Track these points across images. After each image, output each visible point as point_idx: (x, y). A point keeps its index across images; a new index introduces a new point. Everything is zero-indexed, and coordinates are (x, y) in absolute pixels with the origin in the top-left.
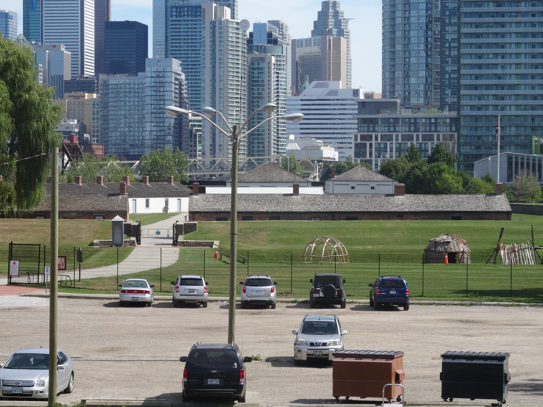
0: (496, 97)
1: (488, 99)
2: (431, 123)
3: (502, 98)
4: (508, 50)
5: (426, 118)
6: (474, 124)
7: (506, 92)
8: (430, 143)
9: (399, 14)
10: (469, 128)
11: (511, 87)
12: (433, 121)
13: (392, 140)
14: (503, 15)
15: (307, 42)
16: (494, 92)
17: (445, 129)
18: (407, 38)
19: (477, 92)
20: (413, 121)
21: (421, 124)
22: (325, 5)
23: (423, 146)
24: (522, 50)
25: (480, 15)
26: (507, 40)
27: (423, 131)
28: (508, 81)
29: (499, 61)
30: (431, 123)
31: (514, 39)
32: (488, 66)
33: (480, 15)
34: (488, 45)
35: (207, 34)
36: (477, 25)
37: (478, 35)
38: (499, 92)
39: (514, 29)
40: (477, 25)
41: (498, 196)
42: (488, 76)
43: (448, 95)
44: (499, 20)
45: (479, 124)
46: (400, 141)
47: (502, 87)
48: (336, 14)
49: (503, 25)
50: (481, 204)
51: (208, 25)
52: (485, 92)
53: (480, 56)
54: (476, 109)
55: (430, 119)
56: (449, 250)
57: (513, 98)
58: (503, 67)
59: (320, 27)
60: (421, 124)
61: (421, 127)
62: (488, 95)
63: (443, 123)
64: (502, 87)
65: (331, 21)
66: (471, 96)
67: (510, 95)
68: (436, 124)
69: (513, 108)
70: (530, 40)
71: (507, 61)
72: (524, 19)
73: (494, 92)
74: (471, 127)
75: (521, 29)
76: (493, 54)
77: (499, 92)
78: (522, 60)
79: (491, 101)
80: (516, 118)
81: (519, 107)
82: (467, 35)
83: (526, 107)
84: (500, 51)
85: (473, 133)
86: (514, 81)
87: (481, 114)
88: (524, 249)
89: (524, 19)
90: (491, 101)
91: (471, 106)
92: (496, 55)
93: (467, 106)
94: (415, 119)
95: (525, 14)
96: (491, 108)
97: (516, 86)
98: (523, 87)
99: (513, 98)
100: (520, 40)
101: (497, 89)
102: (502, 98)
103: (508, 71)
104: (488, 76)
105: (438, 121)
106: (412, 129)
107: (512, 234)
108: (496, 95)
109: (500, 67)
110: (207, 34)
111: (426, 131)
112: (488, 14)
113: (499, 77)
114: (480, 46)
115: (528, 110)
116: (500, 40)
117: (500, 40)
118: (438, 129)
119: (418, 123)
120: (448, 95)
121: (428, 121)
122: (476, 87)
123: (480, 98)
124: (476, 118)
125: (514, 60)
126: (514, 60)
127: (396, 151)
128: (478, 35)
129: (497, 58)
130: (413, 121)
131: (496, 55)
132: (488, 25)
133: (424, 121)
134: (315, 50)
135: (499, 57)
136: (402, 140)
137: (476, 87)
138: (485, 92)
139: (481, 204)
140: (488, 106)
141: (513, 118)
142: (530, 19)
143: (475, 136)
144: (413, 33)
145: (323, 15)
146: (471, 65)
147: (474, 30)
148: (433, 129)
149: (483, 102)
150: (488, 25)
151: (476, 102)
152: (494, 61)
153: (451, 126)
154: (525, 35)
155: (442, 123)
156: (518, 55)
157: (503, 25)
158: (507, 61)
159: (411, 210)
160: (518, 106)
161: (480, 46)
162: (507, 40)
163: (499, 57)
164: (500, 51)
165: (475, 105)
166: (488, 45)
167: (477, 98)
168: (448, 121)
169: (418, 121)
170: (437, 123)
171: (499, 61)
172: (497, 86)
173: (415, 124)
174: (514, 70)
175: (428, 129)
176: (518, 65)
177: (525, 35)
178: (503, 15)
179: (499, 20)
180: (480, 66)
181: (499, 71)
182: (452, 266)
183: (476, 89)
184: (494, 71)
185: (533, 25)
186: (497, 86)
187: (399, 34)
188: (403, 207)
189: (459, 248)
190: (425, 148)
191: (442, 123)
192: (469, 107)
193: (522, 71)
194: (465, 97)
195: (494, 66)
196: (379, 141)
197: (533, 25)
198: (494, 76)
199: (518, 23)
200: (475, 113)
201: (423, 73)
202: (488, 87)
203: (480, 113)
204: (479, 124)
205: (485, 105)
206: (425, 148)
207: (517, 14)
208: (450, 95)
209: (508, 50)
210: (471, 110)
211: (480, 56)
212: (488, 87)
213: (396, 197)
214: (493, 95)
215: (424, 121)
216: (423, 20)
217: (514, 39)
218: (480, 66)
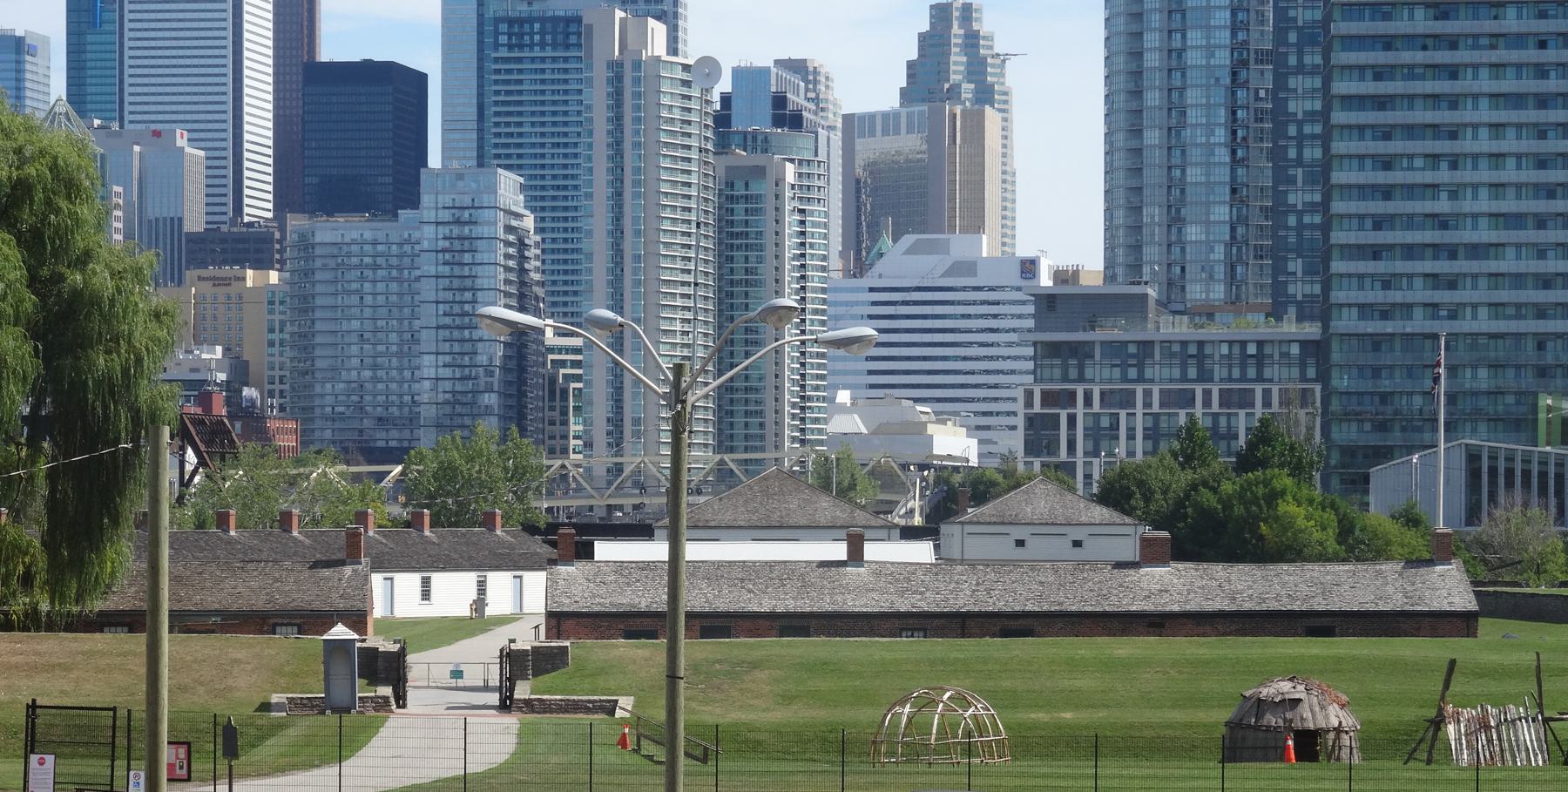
0: (1434, 280)
2: (1245, 356)
3: (1452, 283)
4: (1467, 145)
5: (1231, 343)
6: (1369, 359)
7: (1462, 266)
8: (1242, 413)
9: (1152, 40)
11: (1477, 251)
12: (1252, 349)
14: (1453, 43)
15: (889, 122)
16: (1428, 266)
18: (1176, 109)
19: (1381, 267)
20: (1192, 350)
21: (1217, 357)
22: (940, 15)
23: (1223, 421)
24: (1509, 144)
25: (1388, 43)
26: (1466, 115)
28: (1467, 236)
29: (1444, 175)
30: (1245, 356)
31: (1485, 114)
32: (1411, 191)
33: (1388, 43)
34: (1411, 131)
35: (598, 97)
36: (1379, 74)
38: (1443, 266)
39: (1486, 84)
40: (1379, 74)
41: (1439, 568)
42: (1410, 221)
44: (1443, 57)
45: (1386, 359)
47: (1452, 252)
48: (973, 40)
49: (1453, 72)
50: (1390, 589)
51: (600, 73)
52: (1401, 266)
53: (1387, 163)
55: (1243, 344)
56: (1297, 725)
57: (1483, 282)
58: (1454, 195)
59: (926, 78)
60: (1217, 357)
61: (1217, 367)
62: (1410, 276)
63: (1281, 355)
64: (1452, 252)
65: (957, 61)
66: (1361, 277)
67: (1475, 276)
68: (1260, 359)
69: (1483, 312)
72: (1514, 56)
73: (1428, 266)
74: (1361, 368)
75: (1508, 85)
76: (1426, 156)
77: (1443, 266)
78: (1509, 174)
79: (1420, 294)
81: (1500, 309)
82: (1350, 101)
83: (1520, 310)
85: (1367, 385)
86: (1485, 234)
88: (1513, 721)
89: (1514, 56)
90: (1420, 294)
91: (1361, 306)
92: (1434, 159)
93: (1350, 305)
94: (1201, 344)
95: (1519, 40)
96: (1418, 313)
97: (1492, 250)
99: (1483, 282)
100: (1503, 116)
102: (1452, 283)
103: (1467, 206)
104: (1410, 221)
105: (1267, 350)
106: (1192, 373)
108: (1435, 276)
109: (1444, 195)
110: (598, 97)
111: (1230, 380)
114: (1387, 134)
116: (1444, 116)
117: (1444, 116)
118: (1267, 373)
121: (1236, 350)
122: (1375, 252)
123: (1387, 283)
124: (1377, 342)
125: (1485, 175)
126: (1485, 175)
129: (1435, 168)
130: (1192, 350)
131: (1434, 159)
132: (1411, 72)
133: (1225, 349)
137: (1375, 252)
138: (1401, 266)
139: (1390, 589)
142: (1532, 55)
143: (1372, 394)
145: (933, 44)
146: (1360, 187)
147: (1370, 87)
149: (1396, 296)
150: (1411, 72)
151: (1376, 296)
152: (1428, 177)
153: (1303, 366)
154: (1516, 100)
155: (1276, 357)
156: (1497, 158)
157: (1453, 72)
158: (1466, 175)
159: (1188, 608)
160: (1496, 308)
161: (1387, 134)
162: (1466, 115)
163: (1444, 165)
165: (1371, 305)
166: (1411, 131)
167: (1378, 285)
168: (1295, 350)
169: (1208, 350)
170: (1205, 356)
171: (1444, 175)
172: (1437, 250)
173: (1201, 358)
174: (1484, 204)
175: (1236, 373)
176: (1497, 188)
177: (1516, 100)
178: (1453, 43)
179: (1443, 57)
180: (1387, 192)
181: (1443, 205)
182: (1308, 769)
184: (1429, 206)
185: (1541, 71)
186: (1437, 250)
187: (1153, 98)
188: (1166, 598)
189: (1327, 717)
190: (1229, 427)
191: (1276, 357)
193: (1509, 205)
194: (1345, 281)
195: (1429, 192)
199: (1497, 68)
201: (1222, 213)
202: (1410, 251)
203: (1389, 327)
204: (1386, 359)
206: (1229, 427)
207: (1496, 40)
208: (1300, 274)
209: (1467, 145)
210: (1362, 317)
211: (1387, 163)
212: (1410, 251)
215: (1225, 349)
216: (1223, 58)
217: (1485, 114)
218: (1387, 192)
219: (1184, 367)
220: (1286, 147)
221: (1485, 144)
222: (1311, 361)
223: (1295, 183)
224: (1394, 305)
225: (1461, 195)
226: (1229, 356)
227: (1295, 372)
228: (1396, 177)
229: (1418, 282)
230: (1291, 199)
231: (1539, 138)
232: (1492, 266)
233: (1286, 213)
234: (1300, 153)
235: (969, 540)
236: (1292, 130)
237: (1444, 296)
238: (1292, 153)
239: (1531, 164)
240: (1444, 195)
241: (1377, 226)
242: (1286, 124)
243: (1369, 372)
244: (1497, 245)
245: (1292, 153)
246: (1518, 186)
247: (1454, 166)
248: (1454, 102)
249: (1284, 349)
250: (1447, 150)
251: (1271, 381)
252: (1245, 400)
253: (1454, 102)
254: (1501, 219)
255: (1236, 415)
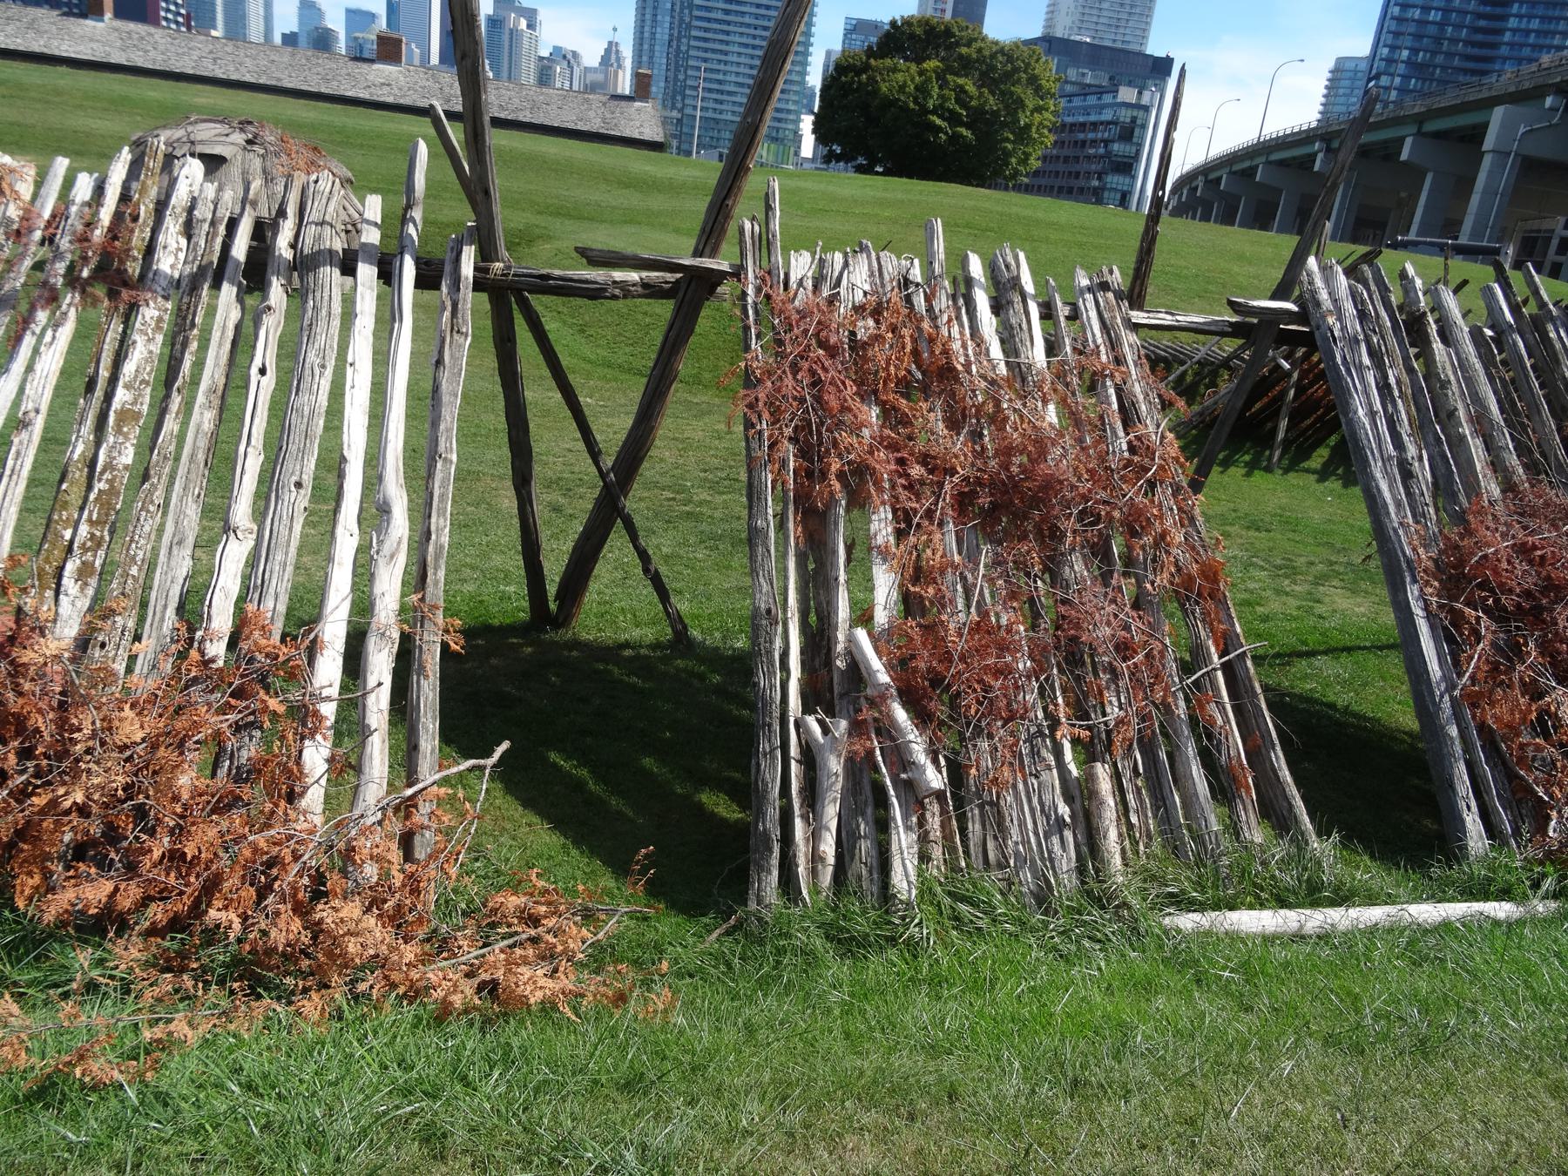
0: (716, 101)
3: (721, 102)
7: (725, 97)
9: (647, 29)
11: (730, 93)
14: (729, 23)
15: (595, 70)
18: (652, 51)
22: (610, 43)
24: (742, 60)
25: (709, 20)
29: (722, 67)
31: (736, 49)
33: (709, 20)
34: (714, 51)
35: (506, 37)
36: (706, 30)
37: (706, 40)
39: (737, 39)
40: (706, 30)
41: (637, 104)
44: (725, 27)
47: (722, 92)
49: (728, 33)
50: (592, 114)
51: (507, 32)
59: (605, 60)
64: (722, 92)
65: (613, 56)
70: (750, 51)
71: (728, 68)
75: (744, 40)
78: (742, 70)
82: (696, 38)
84: (723, 57)
86: (732, 88)
88: (304, 265)
92: (720, 61)
95: (748, 26)
100: (742, 50)
102: (721, 102)
107: (627, 186)
110: (506, 37)
112: (717, 21)
113: (720, 82)
114: (706, 50)
116: (723, 47)
117: (723, 47)
125: (734, 69)
126: (734, 69)
128: (706, 40)
132: (715, 31)
134: (600, 77)
139: (592, 114)
144: (657, 48)
145: (608, 51)
150: (715, 31)
154: (746, 46)
156: (738, 64)
157: (728, 33)
158: (728, 68)
159: (401, 101)
161: (706, 50)
164: (723, 57)
166: (714, 51)
171: (722, 67)
172: (718, 91)
174: (733, 78)
176: (737, 74)
177: (746, 46)
178: (729, 23)
179: (725, 27)
181: (721, 77)
185: (754, 37)
186: (718, 91)
187: (646, 47)
188: (386, 90)
197: (754, 37)
201: (662, 84)
207: (742, 24)
213: (376, 66)
217: (736, 49)
221: (735, 59)
237: (718, 106)
248: (727, 43)
253: (727, 43)
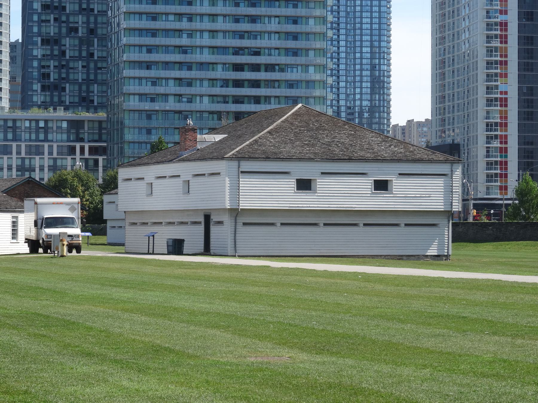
0: (179, 81)
1: (167, 85)
2: (38, 128)
3: (189, 83)
5: (30, 121)
6: (144, 123)
8: (37, 157)
10: (137, 131)
11: (202, 65)
12: (42, 124)
13: (43, 154)
16: (177, 74)
17: (59, 137)
19: (153, 73)
20: (10, 124)
21: (23, 128)
23: (27, 162)
27: (25, 141)
28: (197, 57)
29: (184, 24)
30: (38, 128)
32: (167, 32)
38: (184, 74)
42: (167, 48)
43: (37, 91)
45: (154, 123)
46: (55, 155)
47: (189, 67)
52: (163, 74)
53: (154, 17)
54: (149, 99)
55: (37, 121)
57: (206, 83)
58: (190, 36)
60: (23, 128)
61: (23, 133)
62: (167, 79)
63: (58, 127)
64: (189, 67)
66: (140, 78)
67: (201, 80)
68: (46, 130)
69: (206, 99)
71: (197, 25)
73: (177, 74)
74: (140, 129)
76: (175, 14)
77: (184, 74)
78: (220, 24)
79: (172, 88)
80: (211, 116)
81: (215, 98)
83: (225, 99)
85: (144, 138)
86: (206, 57)
87: (157, 108)
90: (172, 88)
91: (140, 95)
92: (179, 16)
93: (134, 94)
94: (14, 121)
96: (171, 99)
97: (211, 66)
98: (220, 67)
99: (206, 83)
101: (180, 69)
102: (189, 83)
104: (167, 48)
105: (50, 125)
106: (10, 136)
108: (180, 79)
109: (185, 36)
111: (30, 140)
113: (183, 50)
115: (227, 102)
118: (50, 137)
119: (18, 128)
120: (37, 91)
121: (33, 124)
122: (148, 66)
123: (155, 82)
124: (149, 115)
125: (207, 25)
126: (207, 25)
127: (18, 170)
129: (180, 20)
130: (10, 124)
131: (179, 16)
133: (27, 124)
135: (185, 19)
136: (58, 154)
137: (148, 66)
138: (163, 74)
140: (167, 95)
141: (206, 115)
143: (146, 143)
146: (140, 30)
148: (42, 136)
149: (160, 90)
151: (148, 89)
152: (177, 25)
153: (68, 132)
155: (55, 128)
156: (213, 17)
158: (197, 25)
163: (185, 19)
165: (146, 94)
167: (149, 83)
168: (65, 125)
169: (18, 124)
170: (16, 128)
171: (184, 24)
172: (181, 65)
173: (14, 128)
174: (206, 40)
175: (33, 137)
176: (213, 33)
180: (154, 33)
181: (184, 41)
183: (148, 69)
184: (177, 41)
186: (181, 65)
190: (30, 165)
191: (55, 128)
192: (137, 97)
193: (220, 41)
194: (132, 81)
195: (177, 33)
196: (87, 155)
198: (177, 50)
200: (147, 106)
202: (167, 65)
203: (157, 106)
204: (154, 123)
205: (162, 95)
206: (30, 165)
208: (39, 91)
210: (140, 100)
211: (154, 17)
212: (167, 65)
214: (175, 79)
215: (27, 124)
218: (154, 33)
219: (5, 133)
220: (32, 26)
222: (73, 131)
223: (37, 44)
224: (158, 95)
225: (194, 35)
226: (30, 128)
227: (65, 137)
228: (158, 25)
229: (171, 82)
230: (35, 53)
231: (235, 6)
232: (212, 74)
233: (32, 60)
234: (39, 29)
235: (246, 182)
236: (35, 18)
238: (35, 30)
239: (231, 21)
240: (185, 36)
241: (149, 51)
242: (32, 14)
243: (144, 131)
244: (213, 64)
245: (35, 30)
246: (224, 32)
247: (190, 20)
249: (59, 124)
250: (188, 11)
251: (52, 141)
252: (39, 152)
254: (215, 50)
255: (35, 158)
